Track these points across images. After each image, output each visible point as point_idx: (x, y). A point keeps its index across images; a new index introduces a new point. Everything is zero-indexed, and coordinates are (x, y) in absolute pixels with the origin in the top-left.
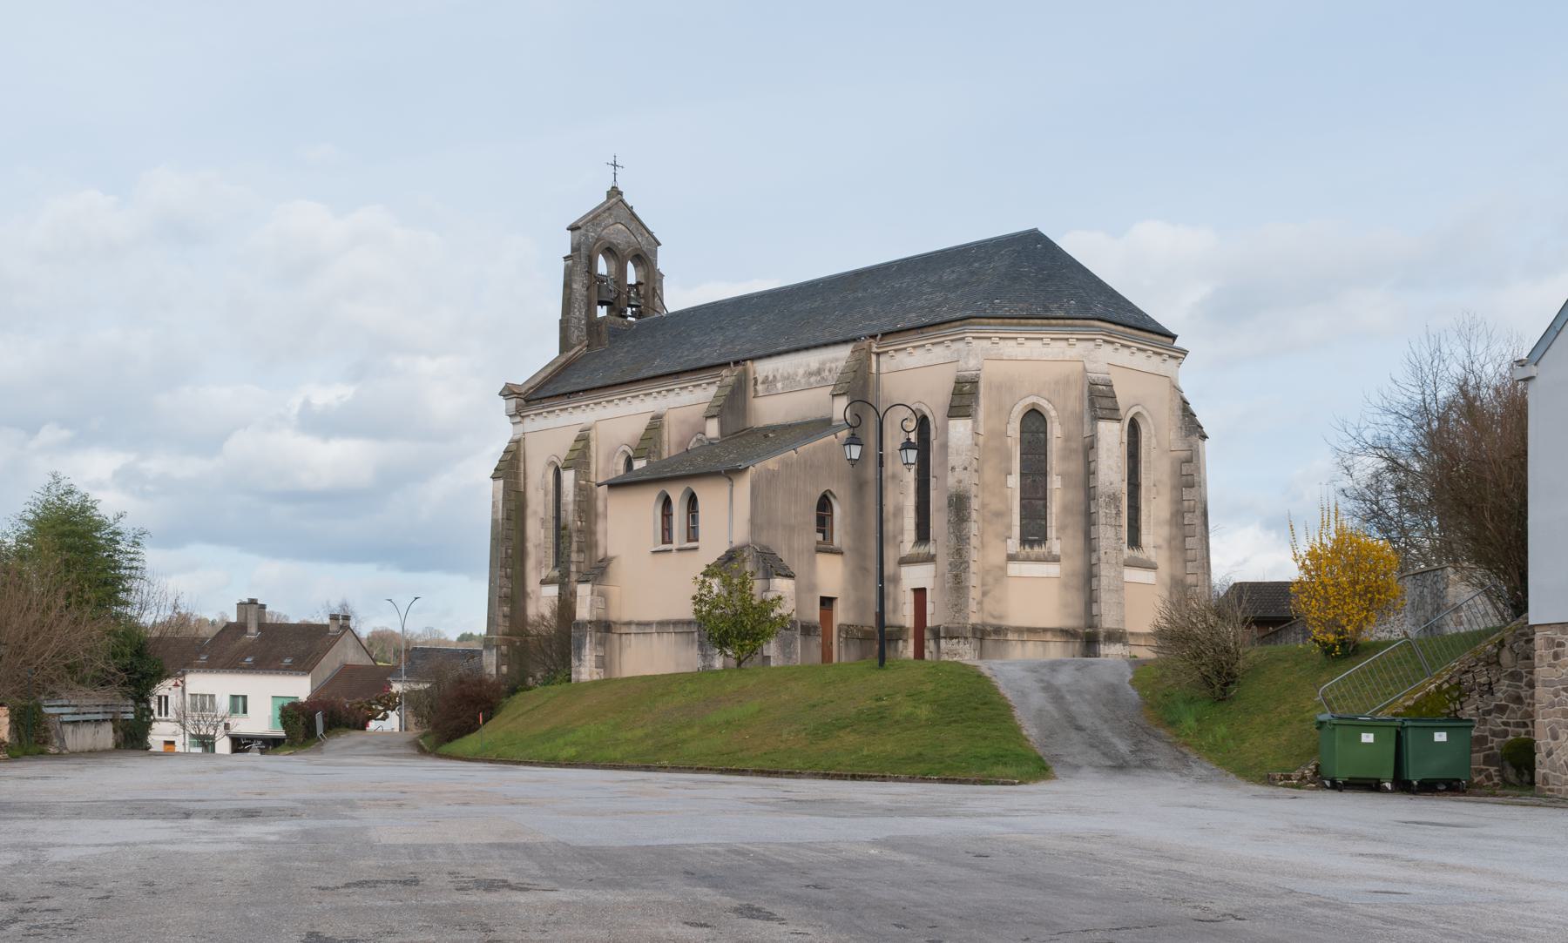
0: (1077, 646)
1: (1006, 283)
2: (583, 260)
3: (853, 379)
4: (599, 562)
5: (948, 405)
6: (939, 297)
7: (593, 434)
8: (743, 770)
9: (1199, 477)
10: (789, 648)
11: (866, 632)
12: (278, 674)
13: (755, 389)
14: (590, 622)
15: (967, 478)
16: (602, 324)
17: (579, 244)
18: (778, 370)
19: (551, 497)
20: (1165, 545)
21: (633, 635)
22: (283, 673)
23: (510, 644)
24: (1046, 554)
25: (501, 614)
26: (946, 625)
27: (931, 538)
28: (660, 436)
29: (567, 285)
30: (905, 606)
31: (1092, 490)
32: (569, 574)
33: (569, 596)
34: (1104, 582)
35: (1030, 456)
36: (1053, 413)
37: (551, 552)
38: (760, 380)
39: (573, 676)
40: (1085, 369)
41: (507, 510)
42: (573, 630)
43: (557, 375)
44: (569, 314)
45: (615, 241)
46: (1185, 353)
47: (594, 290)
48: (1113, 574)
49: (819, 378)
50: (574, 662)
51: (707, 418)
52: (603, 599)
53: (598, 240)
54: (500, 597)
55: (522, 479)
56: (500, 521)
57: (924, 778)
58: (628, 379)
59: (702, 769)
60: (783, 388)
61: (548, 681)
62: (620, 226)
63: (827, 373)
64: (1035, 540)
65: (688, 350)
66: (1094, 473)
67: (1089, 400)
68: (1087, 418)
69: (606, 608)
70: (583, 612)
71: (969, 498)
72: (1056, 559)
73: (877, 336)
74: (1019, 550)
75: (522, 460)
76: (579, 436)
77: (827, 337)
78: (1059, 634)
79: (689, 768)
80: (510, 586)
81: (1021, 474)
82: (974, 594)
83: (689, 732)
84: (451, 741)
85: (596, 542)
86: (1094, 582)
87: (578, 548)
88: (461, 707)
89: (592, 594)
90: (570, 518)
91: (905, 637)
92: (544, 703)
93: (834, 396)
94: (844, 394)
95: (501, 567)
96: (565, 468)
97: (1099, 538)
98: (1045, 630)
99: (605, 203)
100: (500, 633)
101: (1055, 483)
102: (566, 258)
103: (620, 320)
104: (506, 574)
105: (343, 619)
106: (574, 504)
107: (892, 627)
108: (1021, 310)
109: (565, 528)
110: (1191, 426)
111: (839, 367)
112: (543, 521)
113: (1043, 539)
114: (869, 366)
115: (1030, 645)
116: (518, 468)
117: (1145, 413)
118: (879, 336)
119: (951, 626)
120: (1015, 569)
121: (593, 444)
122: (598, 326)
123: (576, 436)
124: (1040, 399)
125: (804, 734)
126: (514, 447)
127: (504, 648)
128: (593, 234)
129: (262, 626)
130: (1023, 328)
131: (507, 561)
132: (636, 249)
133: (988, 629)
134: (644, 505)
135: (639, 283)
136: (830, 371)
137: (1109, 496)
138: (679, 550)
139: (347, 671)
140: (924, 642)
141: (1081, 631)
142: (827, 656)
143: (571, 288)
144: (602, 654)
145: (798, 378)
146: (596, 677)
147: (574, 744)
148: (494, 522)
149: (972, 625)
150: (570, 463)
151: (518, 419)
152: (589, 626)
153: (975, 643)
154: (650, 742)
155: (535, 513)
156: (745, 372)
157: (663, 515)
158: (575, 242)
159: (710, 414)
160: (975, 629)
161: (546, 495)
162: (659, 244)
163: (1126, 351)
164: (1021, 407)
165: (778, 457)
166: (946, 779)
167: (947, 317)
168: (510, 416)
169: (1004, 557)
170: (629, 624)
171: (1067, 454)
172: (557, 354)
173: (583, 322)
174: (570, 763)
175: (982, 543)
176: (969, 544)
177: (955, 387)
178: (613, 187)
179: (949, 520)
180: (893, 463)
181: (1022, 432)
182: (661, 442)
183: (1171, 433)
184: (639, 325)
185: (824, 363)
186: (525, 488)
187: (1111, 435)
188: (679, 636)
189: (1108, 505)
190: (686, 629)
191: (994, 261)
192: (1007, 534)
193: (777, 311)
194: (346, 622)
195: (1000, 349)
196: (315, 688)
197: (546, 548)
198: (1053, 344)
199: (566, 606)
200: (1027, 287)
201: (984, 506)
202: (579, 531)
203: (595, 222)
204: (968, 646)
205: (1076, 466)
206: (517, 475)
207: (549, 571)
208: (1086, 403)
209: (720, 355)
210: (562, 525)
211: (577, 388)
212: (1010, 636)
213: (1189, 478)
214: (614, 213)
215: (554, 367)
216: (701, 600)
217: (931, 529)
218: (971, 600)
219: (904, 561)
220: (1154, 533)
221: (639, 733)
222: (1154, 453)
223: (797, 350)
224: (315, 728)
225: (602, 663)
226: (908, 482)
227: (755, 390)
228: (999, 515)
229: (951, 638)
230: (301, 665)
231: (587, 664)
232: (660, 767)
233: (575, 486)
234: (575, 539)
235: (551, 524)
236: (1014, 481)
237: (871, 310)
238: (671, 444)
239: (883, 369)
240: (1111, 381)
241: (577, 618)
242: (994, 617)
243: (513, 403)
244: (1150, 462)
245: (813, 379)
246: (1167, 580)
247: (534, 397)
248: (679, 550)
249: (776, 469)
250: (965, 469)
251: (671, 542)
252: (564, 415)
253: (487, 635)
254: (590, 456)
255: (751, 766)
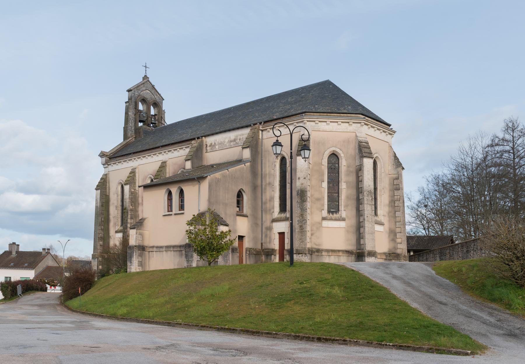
0: (353, 258)
1: (319, 99)
2: (133, 103)
3: (252, 141)
4: (140, 220)
5: (297, 150)
6: (288, 107)
7: (137, 171)
8: (234, 329)
9: (402, 185)
10: (226, 257)
11: (257, 251)
12: (22, 269)
13: (206, 149)
14: (136, 246)
15: (305, 182)
16: (140, 129)
17: (131, 97)
18: (216, 141)
19: (120, 197)
20: (387, 215)
21: (154, 252)
22: (22, 269)
23: (103, 257)
24: (339, 217)
25: (99, 245)
26: (296, 248)
27: (287, 210)
28: (165, 170)
29: (127, 113)
30: (275, 240)
31: (360, 189)
32: (127, 228)
33: (127, 237)
34: (367, 229)
35: (332, 174)
36: (342, 155)
37: (120, 220)
38: (208, 145)
39: (128, 270)
40: (356, 136)
41: (102, 202)
42: (128, 250)
43: (123, 148)
44: (127, 124)
45: (146, 97)
46: (394, 132)
47: (138, 116)
48: (370, 226)
49: (235, 143)
50: (129, 264)
51: (186, 160)
52: (141, 236)
53: (139, 96)
54: (99, 238)
55: (108, 190)
56: (99, 206)
57: (381, 344)
58: (151, 147)
59: (204, 326)
60: (219, 148)
61: (118, 272)
62: (148, 91)
63: (238, 140)
64: (334, 211)
65: (177, 135)
66: (361, 181)
67: (359, 149)
68: (357, 157)
69: (143, 240)
70: (132, 242)
71: (306, 191)
72: (344, 220)
73: (261, 123)
74: (327, 215)
75: (108, 182)
76: (131, 172)
77: (238, 125)
78: (345, 252)
79: (196, 326)
80: (103, 233)
81: (328, 182)
82: (309, 234)
83: (191, 301)
84: (72, 299)
85: (138, 215)
86: (362, 230)
87: (131, 217)
88: (76, 284)
89: (136, 234)
90: (128, 205)
91: (275, 254)
92: (114, 282)
93: (243, 148)
94: (248, 147)
95: (99, 225)
96: (125, 184)
97: (364, 210)
98: (339, 251)
99: (142, 82)
100: (99, 252)
101: (343, 186)
102: (126, 102)
103: (148, 127)
104: (101, 228)
105: (47, 250)
106: (129, 199)
107: (268, 249)
108: (328, 109)
109: (125, 209)
110: (397, 164)
111: (244, 138)
112: (116, 207)
113: (337, 211)
114: (259, 136)
115: (332, 257)
116: (106, 185)
117: (379, 157)
118: (263, 123)
119: (298, 248)
120: (325, 223)
121: (137, 175)
122: (139, 130)
123: (130, 172)
124: (336, 148)
125: (264, 304)
126: (105, 177)
127: (100, 259)
128: (137, 93)
129: (18, 252)
130: (329, 117)
131: (102, 223)
132: (155, 100)
133: (314, 250)
134: (161, 194)
135: (155, 115)
136: (240, 140)
137: (368, 191)
138: (175, 214)
139: (49, 268)
140: (284, 256)
141: (355, 251)
142: (241, 261)
143: (128, 114)
144: (141, 260)
145: (225, 144)
146: (138, 270)
147: (126, 306)
148: (96, 207)
149: (308, 248)
150: (127, 182)
151: (106, 166)
152: (135, 248)
153: (309, 256)
154: (169, 306)
155: (113, 204)
156: (202, 141)
157: (168, 199)
158: (130, 96)
159: (187, 159)
160: (309, 250)
161: (118, 196)
162: (163, 100)
163: (373, 129)
164: (328, 152)
165: (221, 172)
166: (400, 346)
167: (294, 113)
168: (103, 164)
169: (321, 219)
170: (153, 247)
171: (348, 173)
172: (122, 141)
173: (133, 128)
174: (124, 318)
175: (311, 212)
176: (307, 212)
177: (299, 143)
178: (145, 76)
179: (297, 201)
180: (269, 178)
181: (328, 164)
182: (166, 172)
183: (389, 167)
184: (155, 130)
185: (237, 136)
186: (109, 194)
187: (368, 163)
188: (175, 252)
189: (368, 195)
190: (179, 249)
191: (311, 92)
192: (322, 208)
193: (214, 119)
194: (49, 251)
195: (319, 126)
196: (36, 274)
197: (118, 218)
198: (342, 124)
199: (125, 241)
200: (328, 101)
201: (312, 195)
202: (131, 210)
203: (138, 88)
204: (307, 257)
205: (352, 178)
206: (106, 188)
207: (119, 227)
208: (357, 151)
209: (190, 136)
210: (124, 208)
211: (130, 152)
212: (324, 253)
213: (397, 186)
214: (146, 85)
215: (121, 146)
216: (190, 232)
217: (287, 206)
218: (307, 237)
219: (274, 221)
220: (383, 210)
221: (162, 300)
222: (383, 175)
223: (225, 131)
224: (17, 291)
225: (141, 264)
226: (276, 186)
227: (206, 149)
228: (318, 199)
229: (299, 254)
230: (31, 266)
231: (134, 264)
232: (177, 324)
233: (130, 192)
234: (129, 213)
235: (120, 208)
236: (325, 185)
237: (257, 114)
238: (169, 172)
239: (265, 137)
240: (368, 141)
241: (130, 244)
242: (316, 245)
243: (104, 159)
244: (381, 178)
245: (232, 143)
246: (388, 230)
247: (113, 157)
248: (175, 214)
249: (220, 178)
250: (305, 178)
251: (172, 211)
252: (125, 163)
253: (93, 253)
254: (136, 179)
255: (238, 326)
